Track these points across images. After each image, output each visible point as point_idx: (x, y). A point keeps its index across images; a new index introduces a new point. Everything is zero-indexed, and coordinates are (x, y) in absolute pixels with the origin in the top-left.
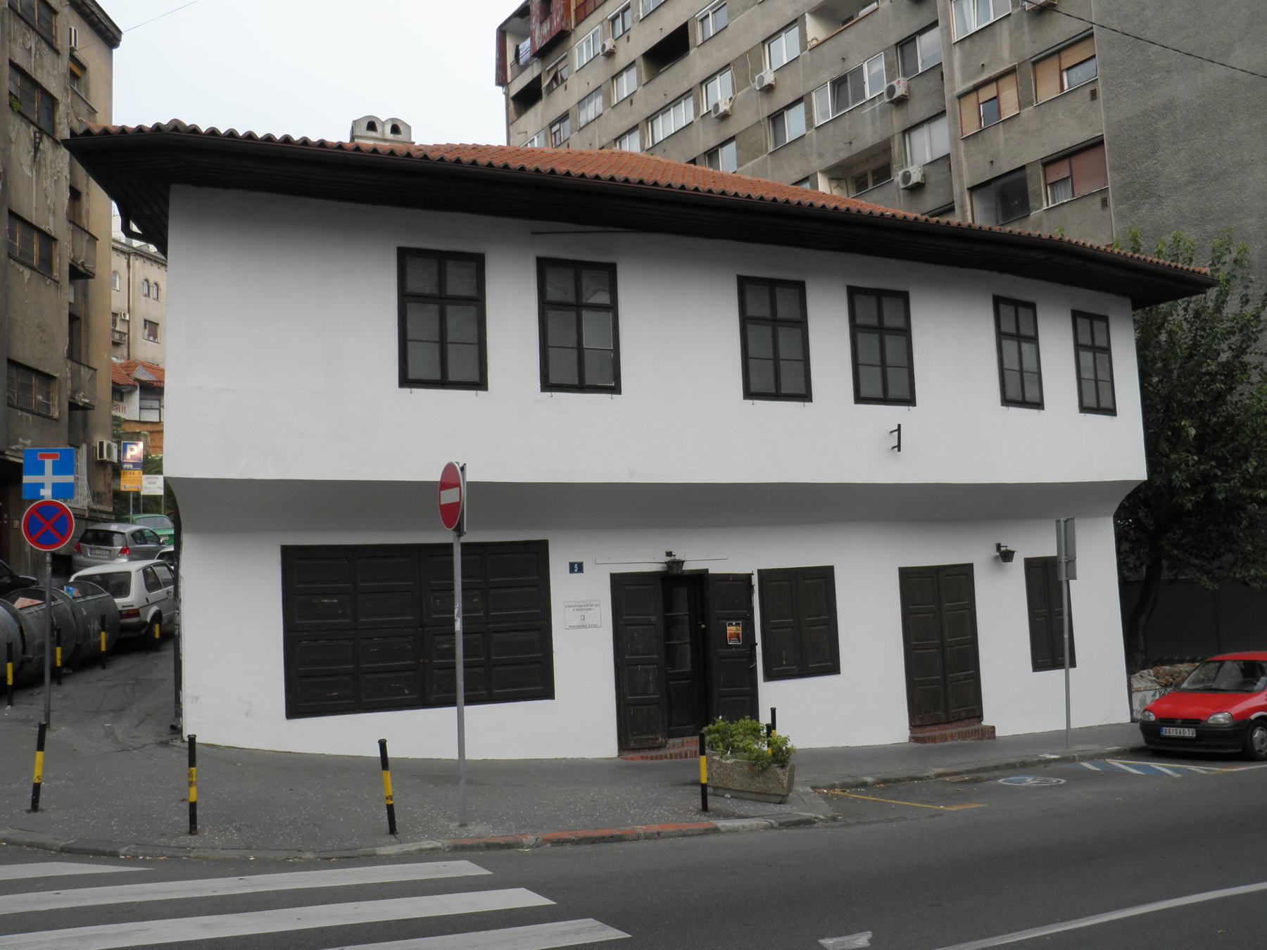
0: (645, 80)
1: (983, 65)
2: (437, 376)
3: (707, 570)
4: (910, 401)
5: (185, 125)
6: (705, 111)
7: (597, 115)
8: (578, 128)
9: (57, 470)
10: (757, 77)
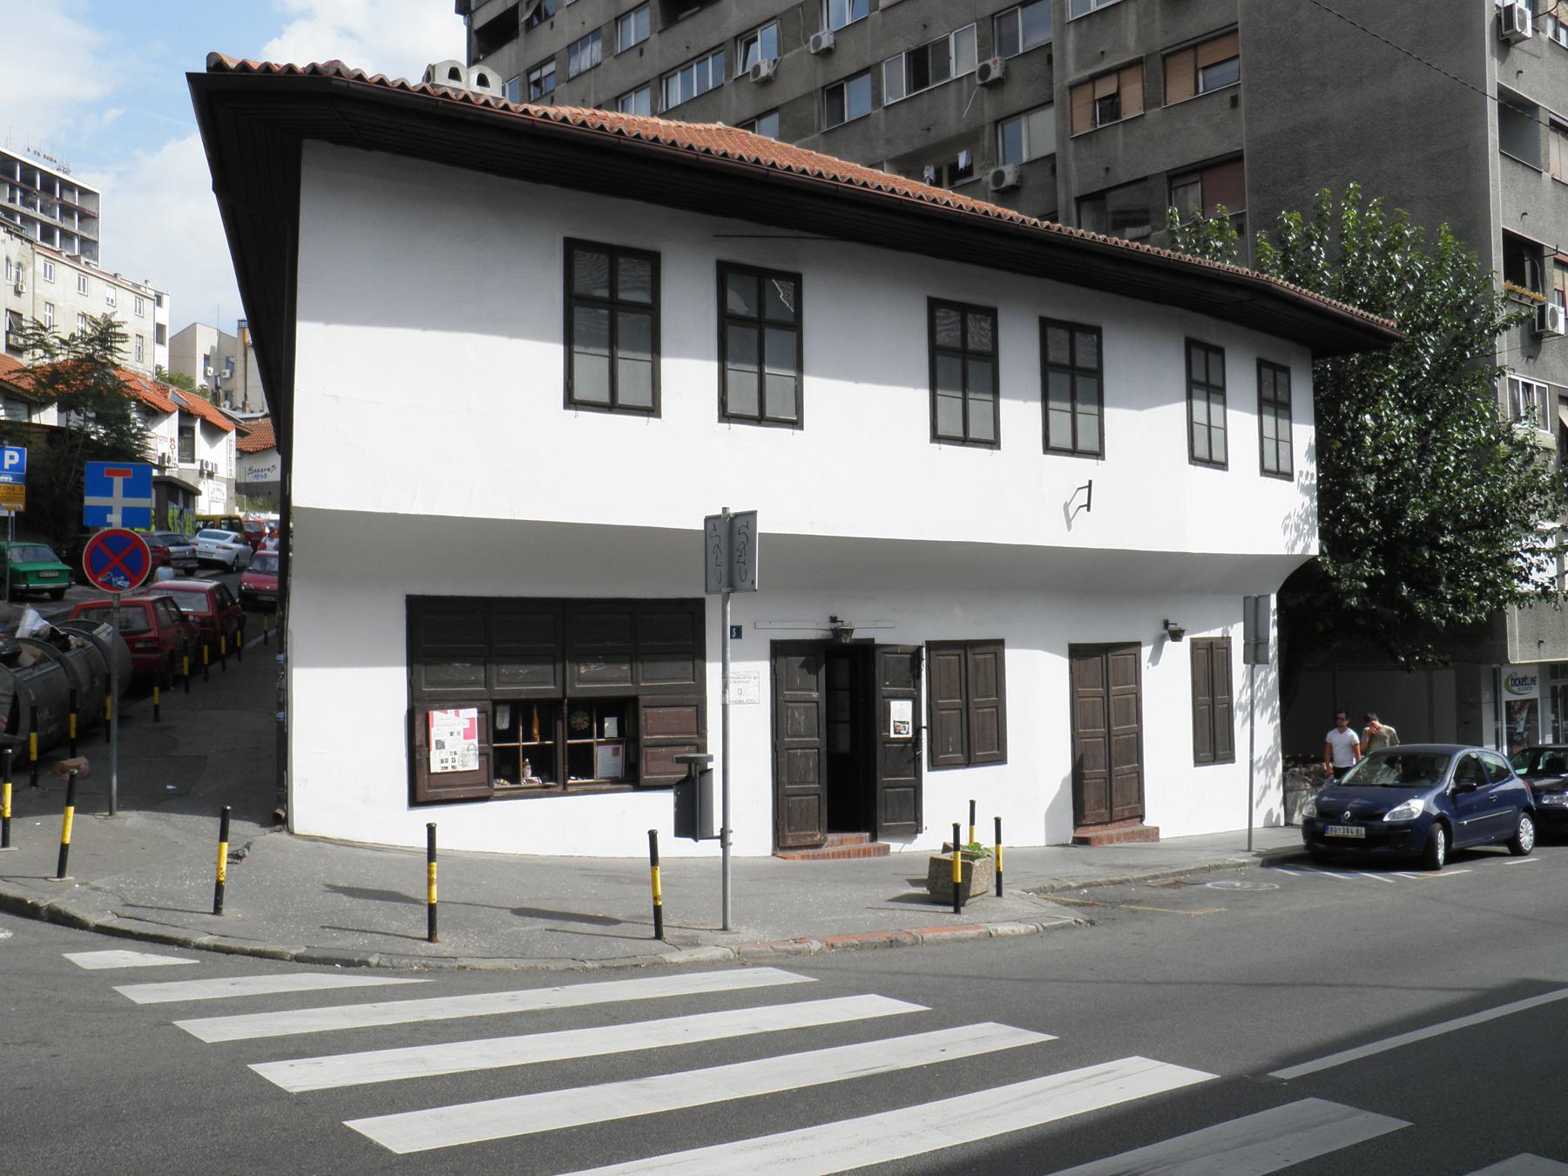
0: (660, 27)
1: (1103, 52)
2: (605, 398)
3: (873, 639)
4: (1099, 454)
5: (348, 70)
6: (740, 74)
7: (594, 64)
8: (567, 79)
9: (128, 493)
10: (812, 38)
